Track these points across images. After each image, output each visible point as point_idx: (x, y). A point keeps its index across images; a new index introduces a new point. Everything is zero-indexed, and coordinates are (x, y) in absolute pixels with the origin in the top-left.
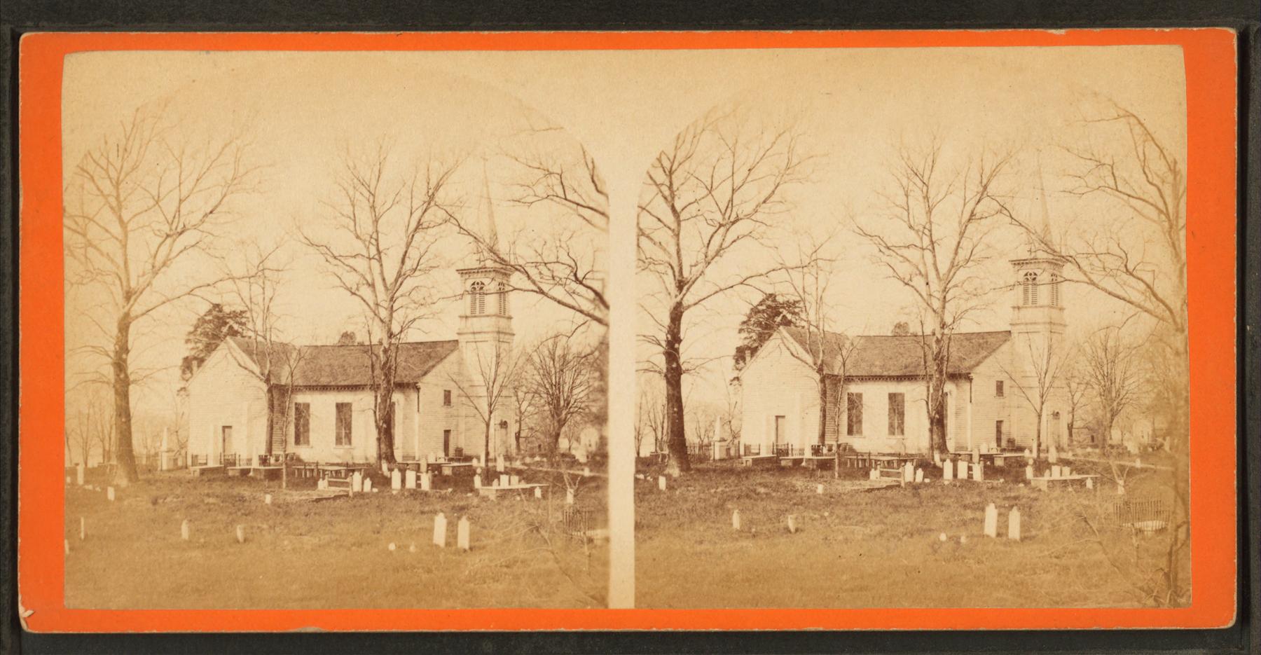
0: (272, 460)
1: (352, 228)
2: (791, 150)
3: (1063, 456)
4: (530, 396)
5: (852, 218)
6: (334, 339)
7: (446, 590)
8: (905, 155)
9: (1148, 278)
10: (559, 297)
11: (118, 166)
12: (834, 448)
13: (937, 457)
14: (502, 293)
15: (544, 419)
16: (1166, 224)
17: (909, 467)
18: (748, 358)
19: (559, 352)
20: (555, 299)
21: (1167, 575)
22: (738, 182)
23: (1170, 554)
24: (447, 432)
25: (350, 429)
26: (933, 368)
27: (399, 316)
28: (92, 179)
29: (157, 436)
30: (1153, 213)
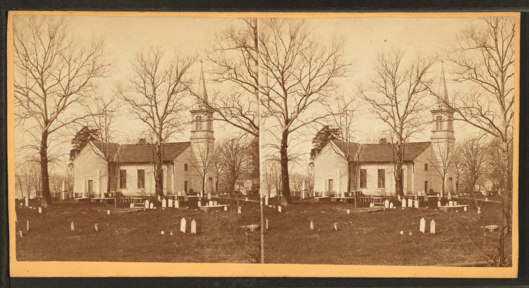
0: (350, 195)
1: (144, 92)
3: (454, 197)
5: (362, 92)
7: (186, 251)
9: (491, 118)
11: (42, 66)
12: (354, 194)
14: (210, 121)
16: (499, 94)
17: (387, 202)
18: (317, 154)
21: (499, 249)
22: (312, 76)
23: (501, 240)
25: (144, 181)
27: (405, 131)
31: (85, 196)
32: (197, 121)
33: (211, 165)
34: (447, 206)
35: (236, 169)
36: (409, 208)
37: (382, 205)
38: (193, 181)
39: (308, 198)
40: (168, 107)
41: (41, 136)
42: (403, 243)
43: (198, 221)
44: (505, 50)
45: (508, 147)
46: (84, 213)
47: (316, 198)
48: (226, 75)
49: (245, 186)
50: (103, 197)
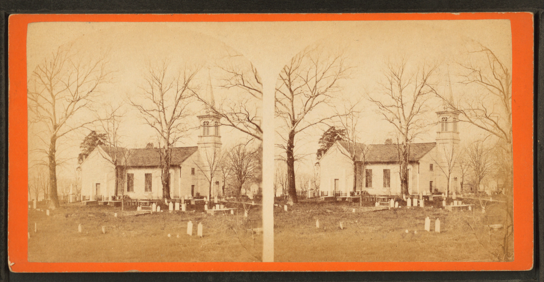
3: (459, 196)
6: (144, 146)
9: (495, 120)
12: (360, 193)
13: (404, 197)
14: (216, 126)
16: (503, 97)
18: (323, 154)
21: (503, 248)
23: (505, 238)
24: (193, 186)
25: (151, 185)
26: (402, 158)
27: (172, 136)
28: (40, 77)
29: (68, 188)
30: (497, 92)
33: (218, 169)
35: (242, 173)
36: (176, 211)
37: (150, 209)
41: (50, 140)
42: (409, 241)
46: (91, 215)
49: (251, 190)
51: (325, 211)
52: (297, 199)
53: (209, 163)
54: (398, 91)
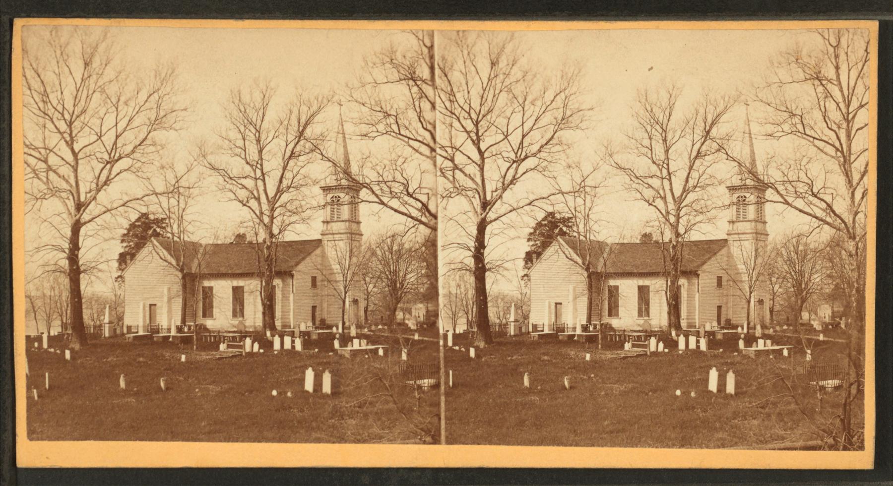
1: (243, 156)
2: (159, 106)
3: (766, 332)
4: (374, 281)
8: (649, 109)
9: (828, 199)
10: (396, 207)
12: (598, 327)
15: (385, 297)
16: (842, 159)
18: (534, 260)
19: (395, 248)
20: (392, 208)
21: (842, 421)
23: (845, 405)
25: (243, 306)
27: (683, 221)
28: (51, 120)
30: (831, 150)
31: (144, 331)
32: (332, 203)
34: (754, 348)
36: (691, 350)
37: (645, 346)
38: (325, 305)
39: (520, 334)
40: (284, 180)
42: (681, 410)
43: (334, 374)
44: (852, 84)
45: (857, 248)
46: (141, 359)
47: (533, 334)
48: (381, 127)
50: (173, 333)
51: (539, 359)
52: (491, 337)
53: (746, 267)
54: (663, 151)
